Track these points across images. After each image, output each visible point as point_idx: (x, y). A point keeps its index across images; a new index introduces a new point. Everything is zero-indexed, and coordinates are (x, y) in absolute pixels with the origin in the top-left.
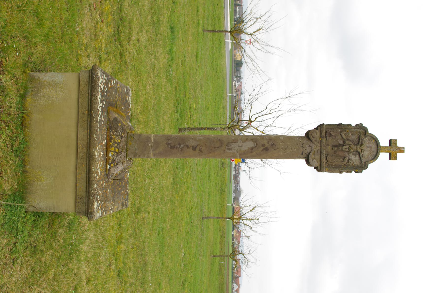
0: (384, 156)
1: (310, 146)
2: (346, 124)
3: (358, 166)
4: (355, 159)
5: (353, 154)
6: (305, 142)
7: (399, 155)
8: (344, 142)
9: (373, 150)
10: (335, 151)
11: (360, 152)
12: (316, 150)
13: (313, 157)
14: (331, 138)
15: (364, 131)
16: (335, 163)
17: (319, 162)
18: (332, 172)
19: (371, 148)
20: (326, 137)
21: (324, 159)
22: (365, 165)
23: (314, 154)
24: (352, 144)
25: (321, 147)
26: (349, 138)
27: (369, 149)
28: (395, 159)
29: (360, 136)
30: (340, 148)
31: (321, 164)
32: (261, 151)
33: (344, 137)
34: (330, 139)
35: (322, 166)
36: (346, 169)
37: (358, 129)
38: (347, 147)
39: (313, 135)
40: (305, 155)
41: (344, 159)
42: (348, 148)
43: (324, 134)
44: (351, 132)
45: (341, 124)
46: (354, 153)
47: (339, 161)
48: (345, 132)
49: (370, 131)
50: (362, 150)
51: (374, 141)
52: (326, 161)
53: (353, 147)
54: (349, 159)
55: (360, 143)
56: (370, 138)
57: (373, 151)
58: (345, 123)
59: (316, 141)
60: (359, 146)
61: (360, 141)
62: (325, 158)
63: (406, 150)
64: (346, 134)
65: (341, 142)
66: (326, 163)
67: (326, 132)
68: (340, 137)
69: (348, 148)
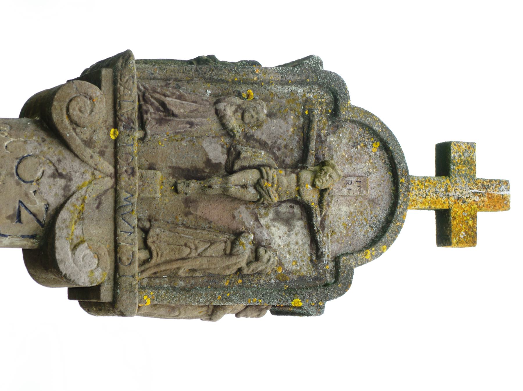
0: (418, 224)
1: (57, 174)
2: (236, 59)
3: (302, 278)
4: (286, 243)
5: (278, 218)
6: (30, 149)
7: (486, 221)
8: (233, 154)
9: (372, 193)
10: (188, 202)
11: (314, 204)
12: (91, 194)
13: (77, 231)
14: (167, 129)
15: (328, 98)
16: (188, 265)
17: (108, 262)
18: (172, 311)
19: (362, 182)
20: (143, 126)
21: (131, 243)
22: (336, 274)
23: (81, 218)
24: (272, 162)
25: (116, 176)
26: (258, 134)
27: (354, 187)
28: (471, 239)
29: (309, 121)
30: (216, 182)
31: (116, 269)
32: (100, 89)
33: (234, 123)
34: (160, 134)
35: (125, 281)
36: (243, 298)
37: (301, 83)
38: (252, 176)
39: (75, 113)
40: (29, 225)
41: (233, 243)
42: (257, 185)
43: (129, 107)
44: (265, 100)
45: (212, 58)
46: (284, 209)
47: (209, 256)
48: (238, 101)
49: (358, 97)
50: (322, 192)
51: (374, 149)
52: (143, 255)
53: (282, 181)
54: (257, 245)
55: (311, 159)
56: (358, 131)
57: (373, 202)
58: (228, 54)
59: (89, 143)
60: (306, 176)
61: (313, 145)
62: (137, 236)
63: (514, 195)
64: (242, 111)
65: (217, 153)
66: (145, 262)
67: (143, 98)
68: (215, 126)
69: (257, 185)
